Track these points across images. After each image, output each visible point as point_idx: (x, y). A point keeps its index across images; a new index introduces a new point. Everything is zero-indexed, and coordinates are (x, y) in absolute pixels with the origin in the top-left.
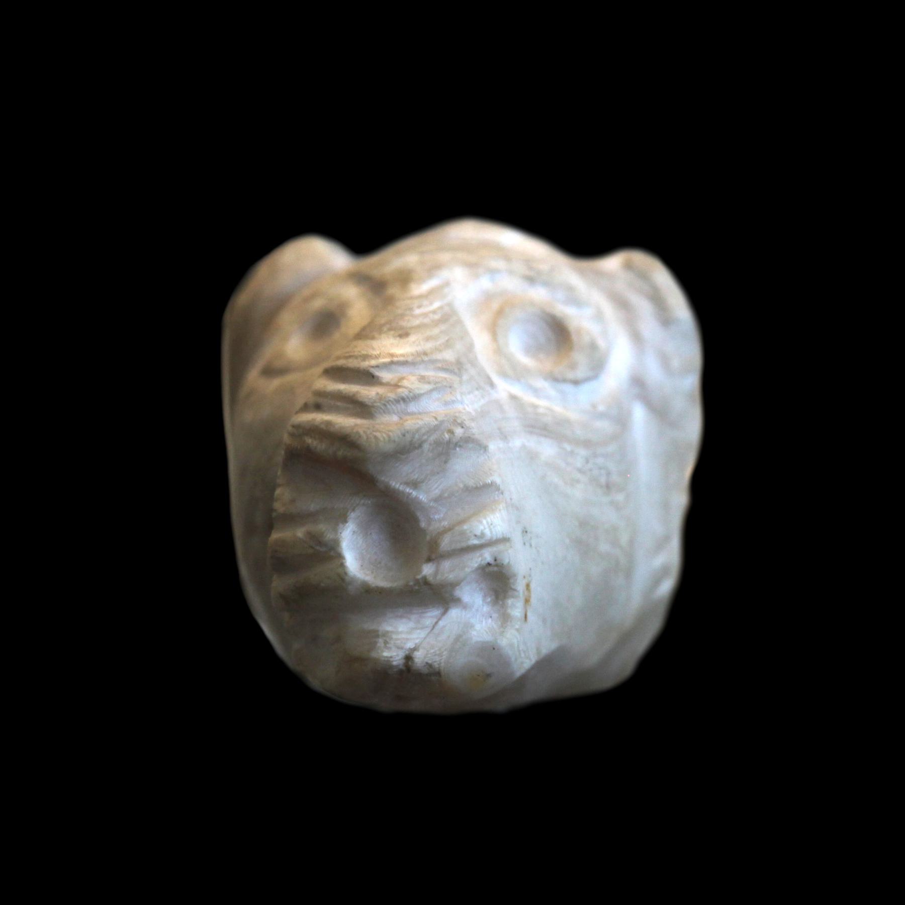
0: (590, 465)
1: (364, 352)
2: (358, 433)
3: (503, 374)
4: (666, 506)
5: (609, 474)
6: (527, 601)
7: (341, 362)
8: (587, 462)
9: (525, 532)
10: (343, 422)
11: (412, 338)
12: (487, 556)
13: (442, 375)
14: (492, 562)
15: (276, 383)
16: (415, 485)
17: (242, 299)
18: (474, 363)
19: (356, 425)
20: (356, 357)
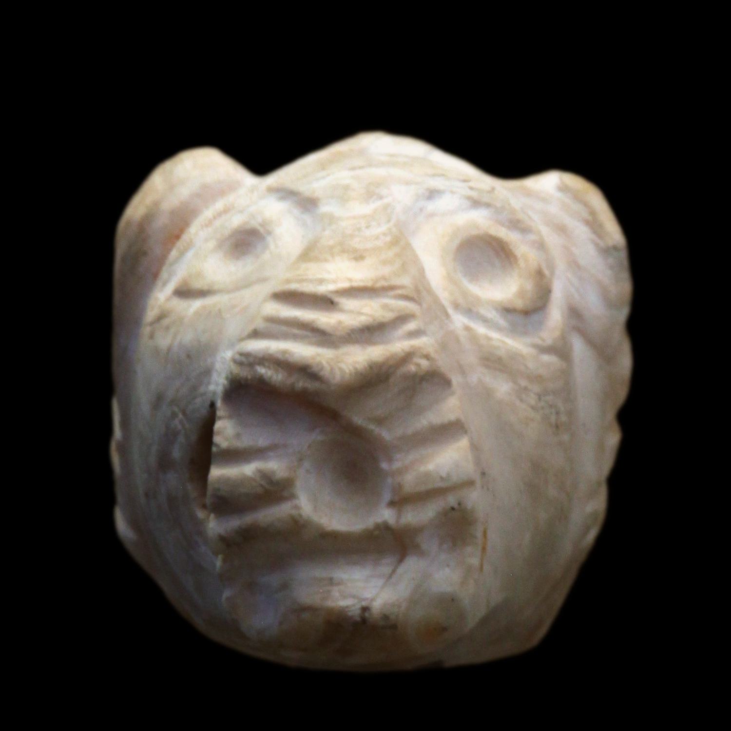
0: (542, 404)
1: (319, 276)
2: (320, 364)
3: (456, 306)
4: (601, 446)
5: (557, 413)
6: (484, 549)
7: (294, 286)
8: (540, 399)
9: (483, 474)
10: (302, 351)
11: (368, 261)
12: (451, 500)
13: (402, 304)
14: (456, 506)
15: (196, 304)
16: (380, 421)
17: (137, 208)
18: (429, 291)
19: (319, 355)
20: (311, 281)
